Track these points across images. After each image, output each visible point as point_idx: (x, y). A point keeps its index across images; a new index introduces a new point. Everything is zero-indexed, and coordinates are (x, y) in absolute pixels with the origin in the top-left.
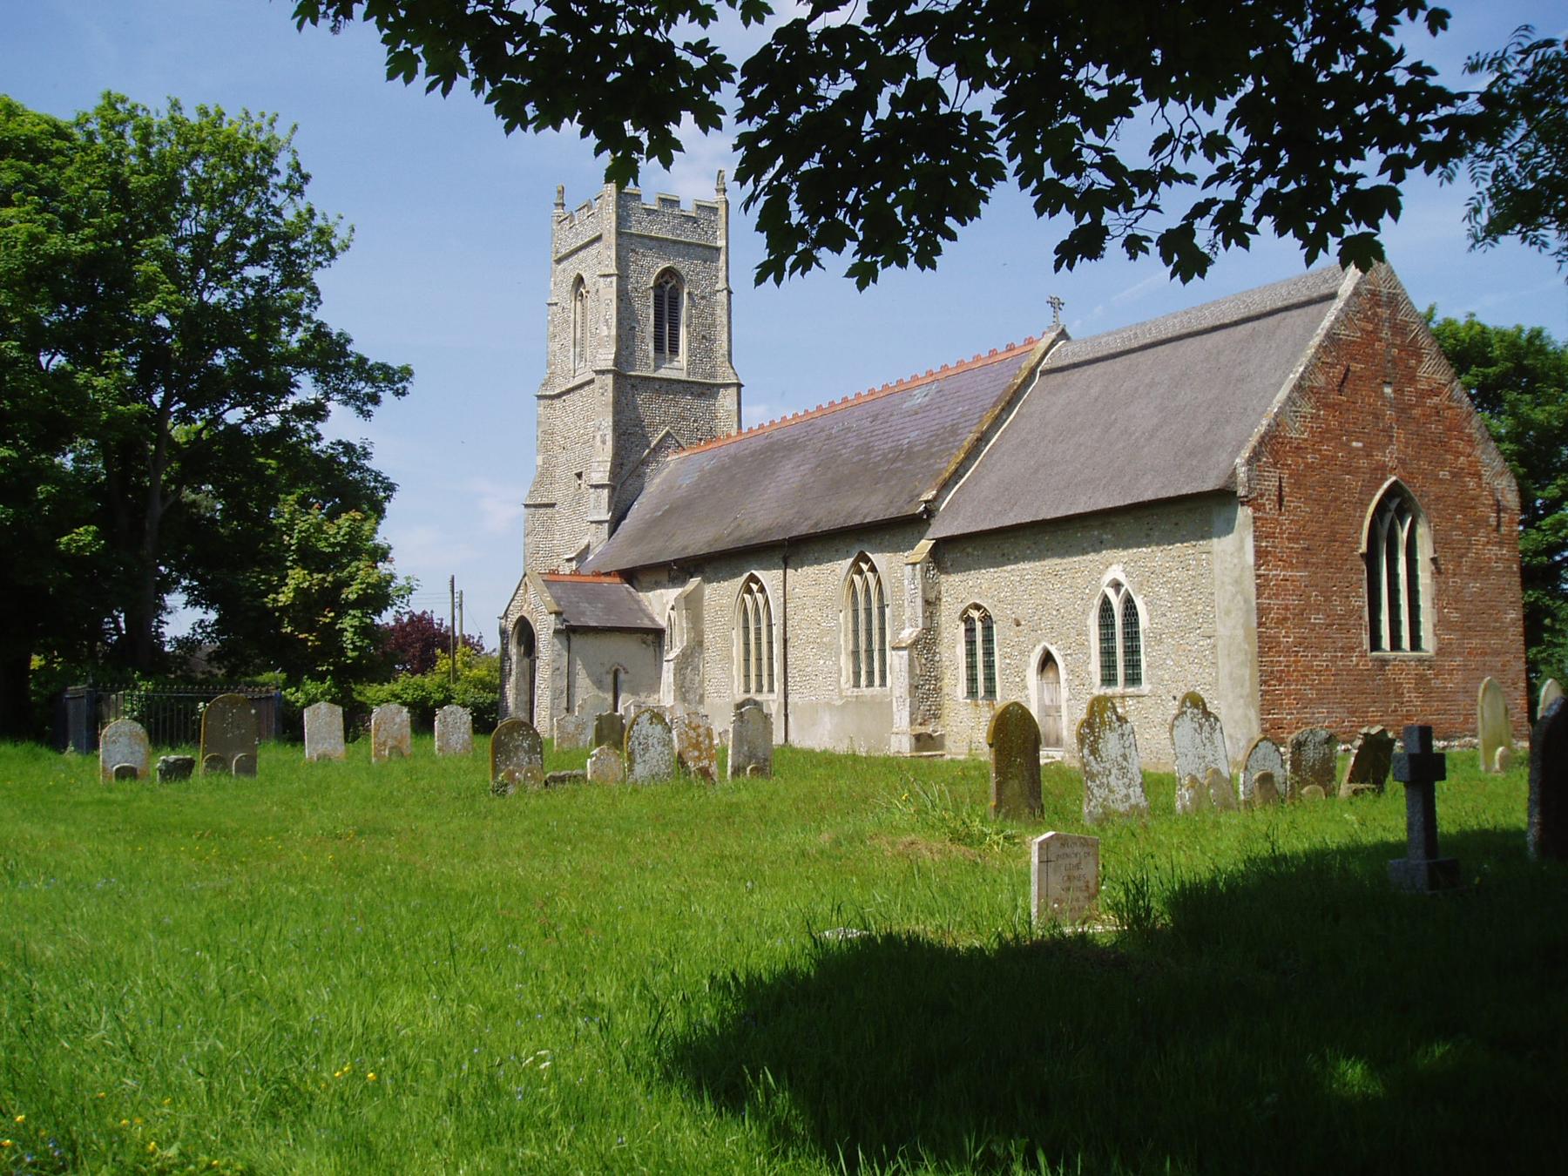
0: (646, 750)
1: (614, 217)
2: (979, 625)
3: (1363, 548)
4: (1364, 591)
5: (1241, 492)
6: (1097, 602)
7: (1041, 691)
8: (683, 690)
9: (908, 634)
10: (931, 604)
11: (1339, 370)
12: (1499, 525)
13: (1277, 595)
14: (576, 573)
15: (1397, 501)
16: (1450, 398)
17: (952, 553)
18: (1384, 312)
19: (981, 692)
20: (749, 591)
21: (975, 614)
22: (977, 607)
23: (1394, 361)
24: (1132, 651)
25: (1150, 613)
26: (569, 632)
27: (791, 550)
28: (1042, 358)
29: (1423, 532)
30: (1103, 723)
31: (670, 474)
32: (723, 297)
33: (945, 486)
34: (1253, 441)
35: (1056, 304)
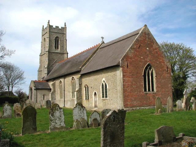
0: (6, 110)
1: (49, 29)
2: (87, 88)
3: (143, 74)
4: (143, 82)
5: (121, 65)
6: (101, 84)
7: (95, 99)
8: (52, 98)
9: (77, 89)
10: (80, 85)
11: (139, 45)
12: (168, 71)
13: (127, 83)
14: (42, 81)
15: (149, 67)
16: (159, 50)
17: (83, 75)
18: (147, 36)
19: (87, 98)
20: (60, 83)
21: (86, 86)
22: (87, 85)
23: (149, 44)
24: (106, 92)
25: (108, 86)
26: (37, 89)
27: (65, 76)
28: (100, 46)
29: (154, 72)
30: (56, 109)
31: (56, 66)
32: (65, 41)
33: (83, 66)
34: (123, 57)
35: (103, 38)
